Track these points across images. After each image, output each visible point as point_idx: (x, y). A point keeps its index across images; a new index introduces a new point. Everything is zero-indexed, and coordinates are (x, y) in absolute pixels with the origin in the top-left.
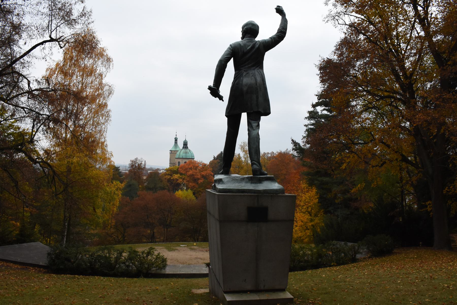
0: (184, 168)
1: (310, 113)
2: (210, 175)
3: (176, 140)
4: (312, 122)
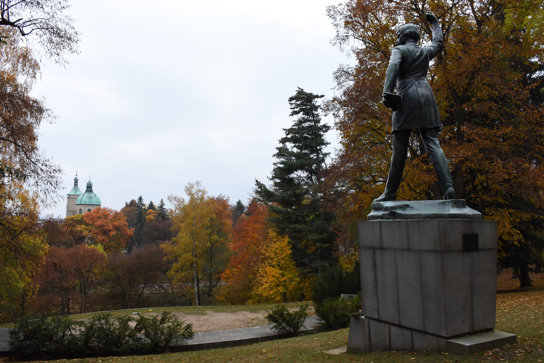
0: (90, 217)
1: (279, 149)
2: (124, 226)
3: (76, 181)
4: (282, 159)
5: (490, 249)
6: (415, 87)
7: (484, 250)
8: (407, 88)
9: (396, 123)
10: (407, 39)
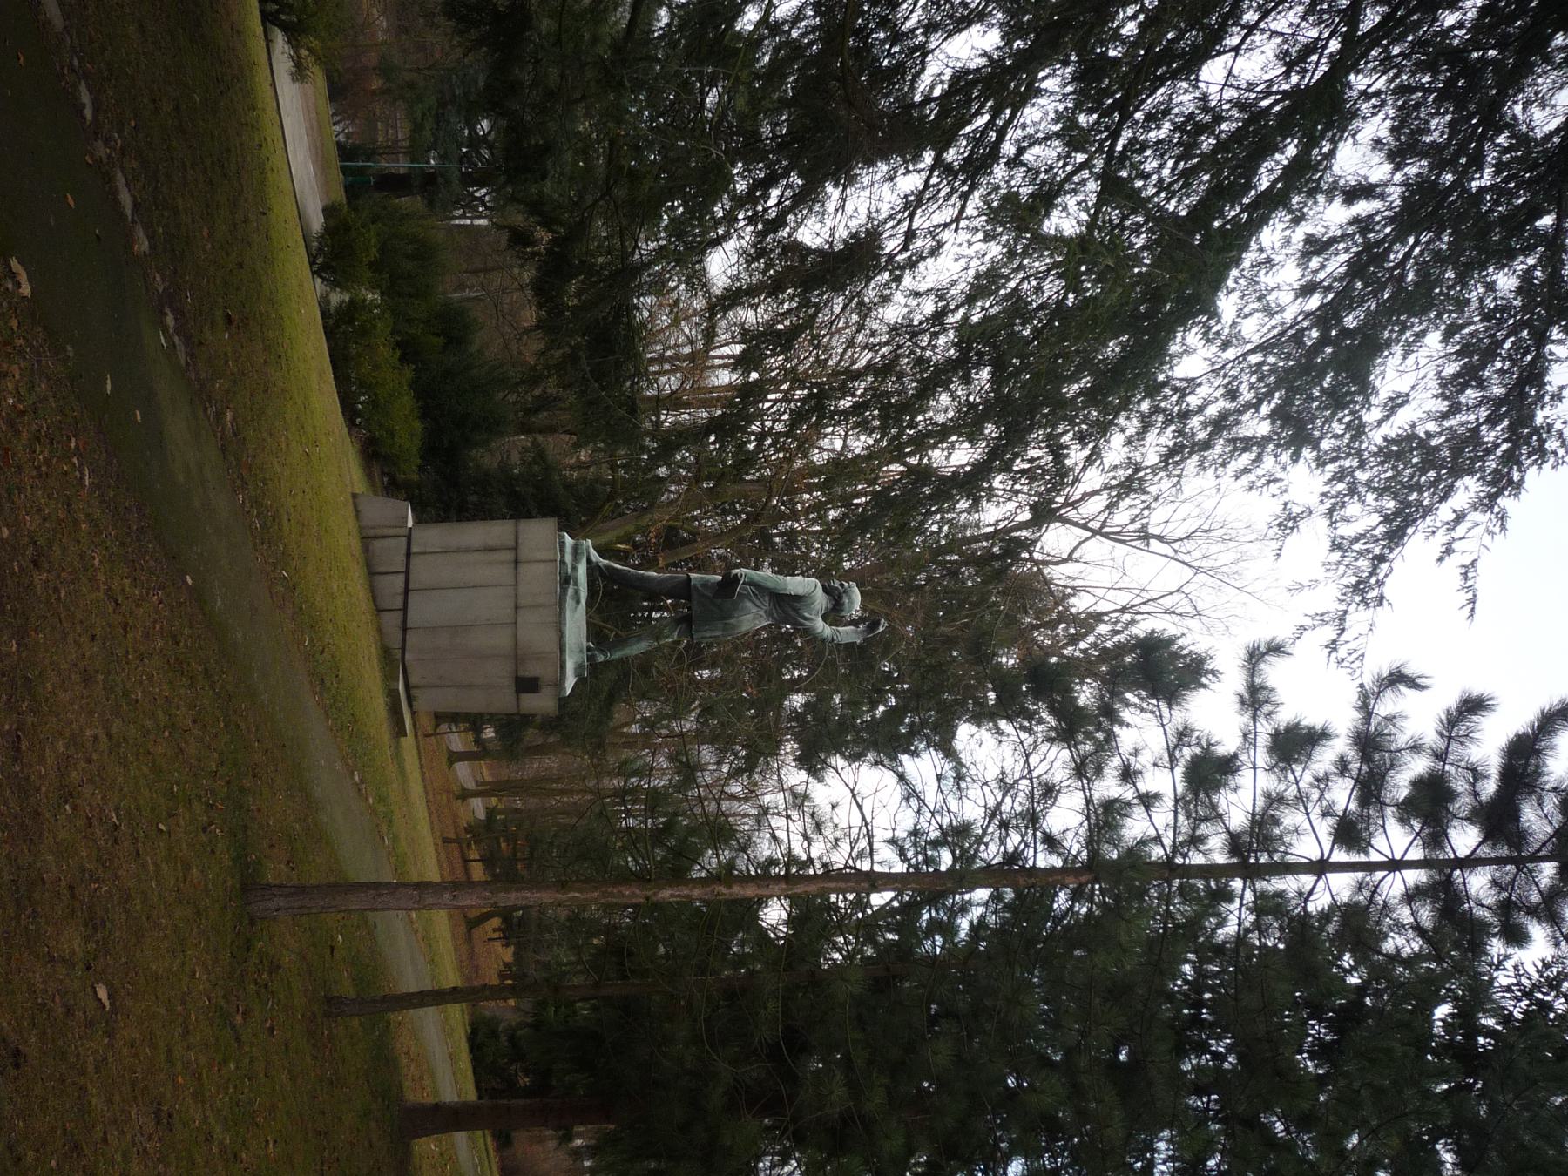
7: (518, 698)
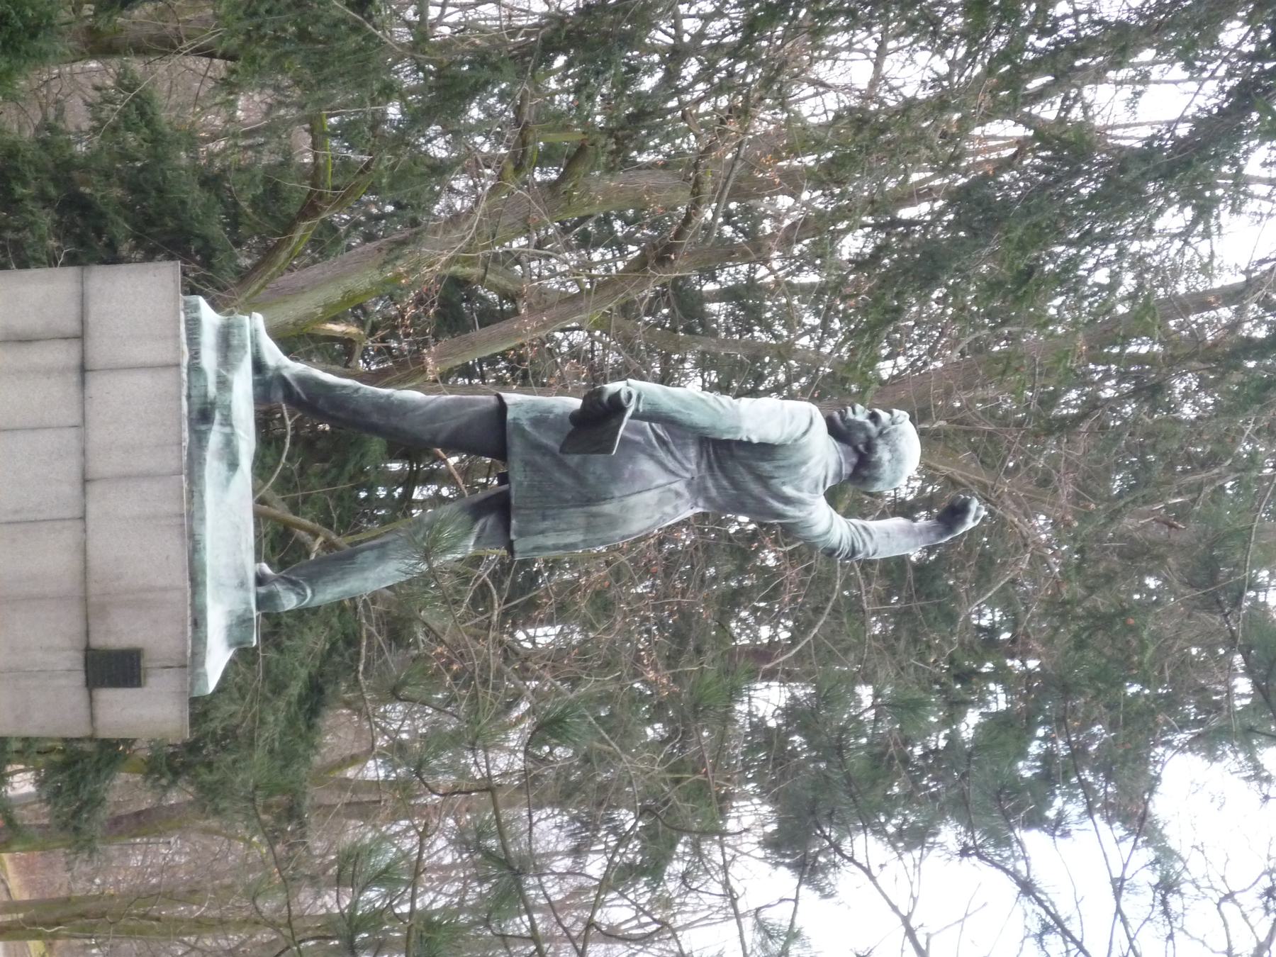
5: (92, 718)
6: (661, 481)
7: (91, 700)
8: (661, 454)
9: (532, 415)
10: (856, 449)
